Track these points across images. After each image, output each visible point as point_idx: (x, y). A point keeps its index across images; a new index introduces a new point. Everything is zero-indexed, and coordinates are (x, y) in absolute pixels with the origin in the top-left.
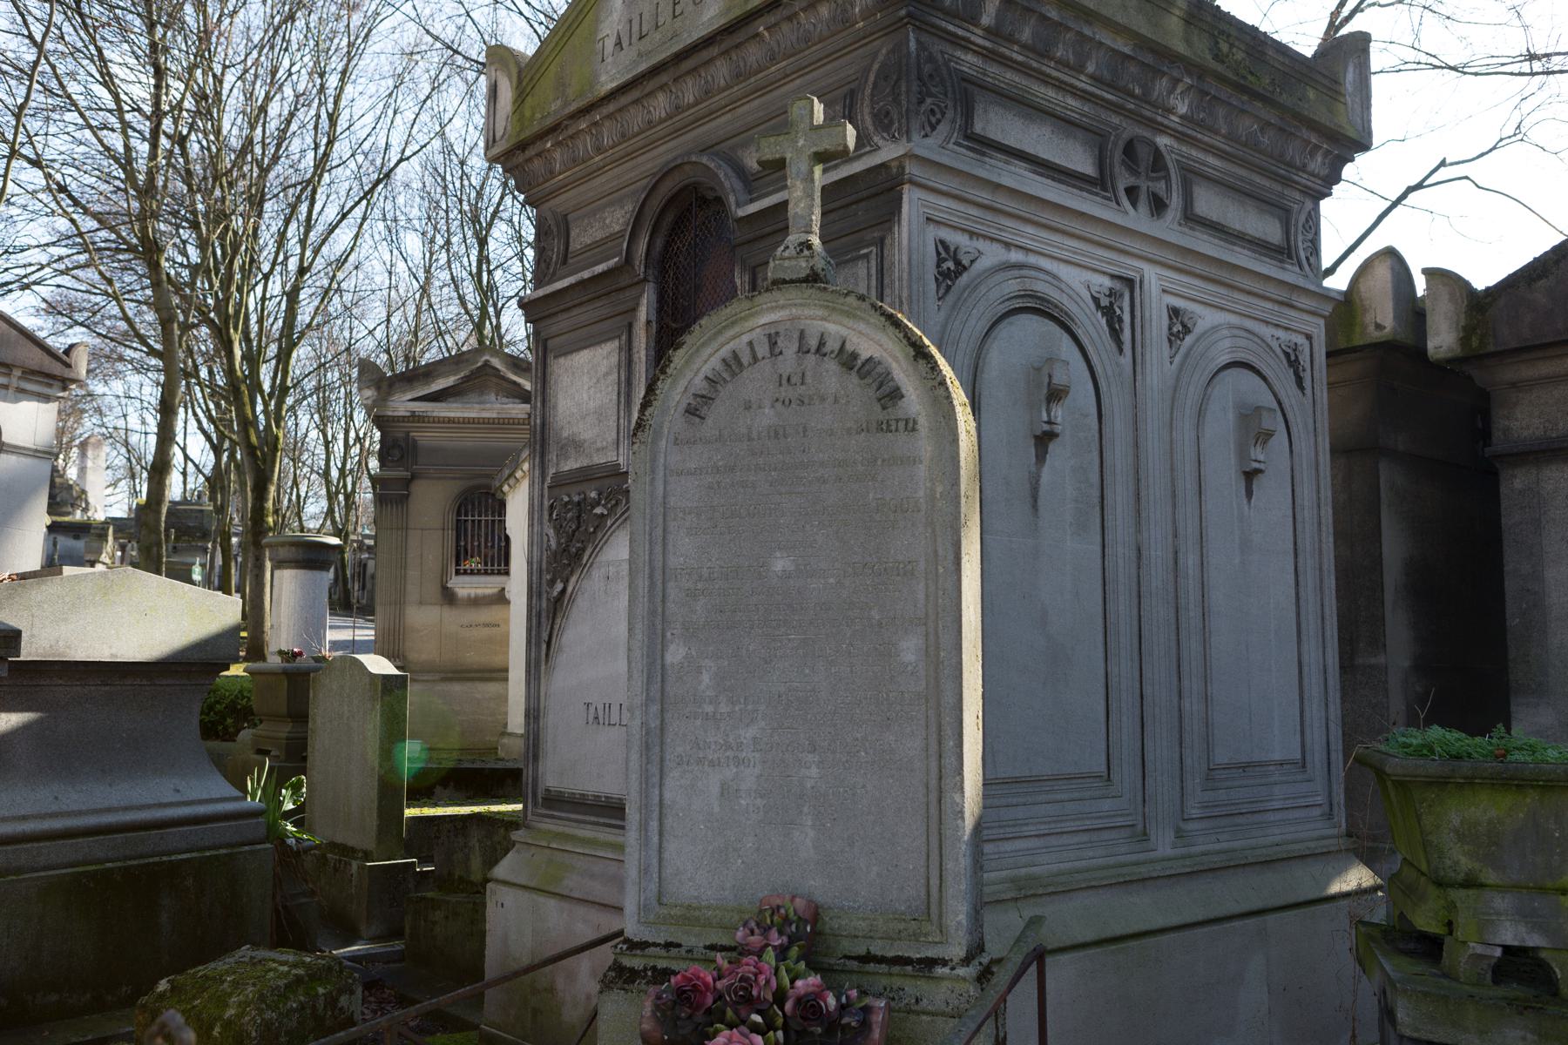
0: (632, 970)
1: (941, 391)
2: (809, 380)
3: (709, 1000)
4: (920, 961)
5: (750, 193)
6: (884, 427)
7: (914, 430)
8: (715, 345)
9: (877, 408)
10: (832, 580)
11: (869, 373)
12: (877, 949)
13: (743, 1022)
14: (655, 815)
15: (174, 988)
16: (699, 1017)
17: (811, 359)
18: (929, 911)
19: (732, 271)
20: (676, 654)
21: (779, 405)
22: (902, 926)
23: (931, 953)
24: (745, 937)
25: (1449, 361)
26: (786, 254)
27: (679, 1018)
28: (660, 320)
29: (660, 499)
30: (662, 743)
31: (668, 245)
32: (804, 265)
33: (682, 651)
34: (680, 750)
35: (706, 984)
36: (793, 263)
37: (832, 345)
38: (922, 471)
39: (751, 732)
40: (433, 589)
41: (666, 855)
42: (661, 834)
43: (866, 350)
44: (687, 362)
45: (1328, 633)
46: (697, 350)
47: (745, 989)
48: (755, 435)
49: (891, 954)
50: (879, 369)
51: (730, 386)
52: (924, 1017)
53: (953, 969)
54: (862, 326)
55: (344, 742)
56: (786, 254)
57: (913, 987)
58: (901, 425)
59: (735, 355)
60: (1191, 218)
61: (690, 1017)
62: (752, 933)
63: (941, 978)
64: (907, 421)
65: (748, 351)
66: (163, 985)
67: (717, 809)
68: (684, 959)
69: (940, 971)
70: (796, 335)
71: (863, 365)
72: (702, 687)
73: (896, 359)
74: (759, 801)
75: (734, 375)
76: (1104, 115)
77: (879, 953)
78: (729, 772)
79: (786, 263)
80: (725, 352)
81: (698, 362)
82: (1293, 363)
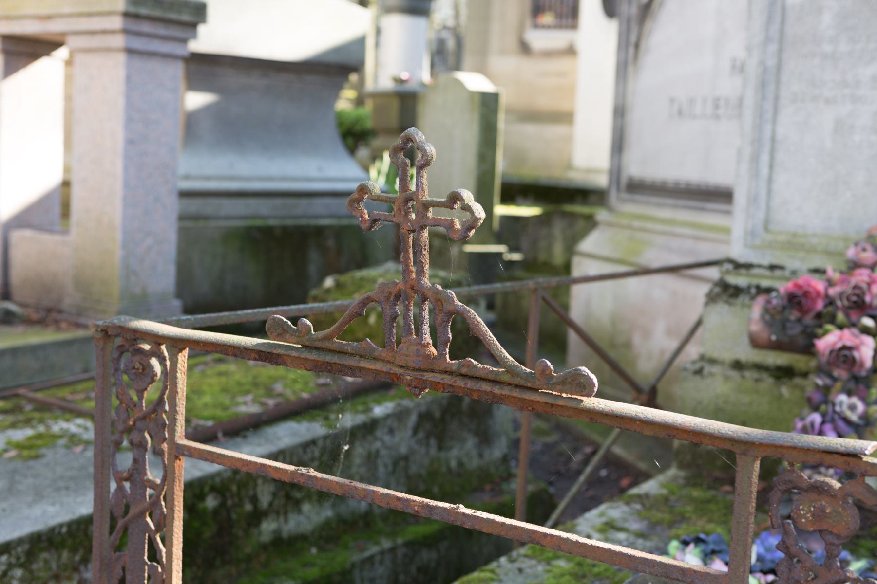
3: (820, 305)
13: (853, 325)
14: (767, 149)
15: (339, 286)
16: (809, 320)
24: (857, 254)
27: (788, 320)
40: (512, 41)
42: (771, 167)
47: (858, 296)
61: (799, 320)
62: (864, 250)
66: (329, 282)
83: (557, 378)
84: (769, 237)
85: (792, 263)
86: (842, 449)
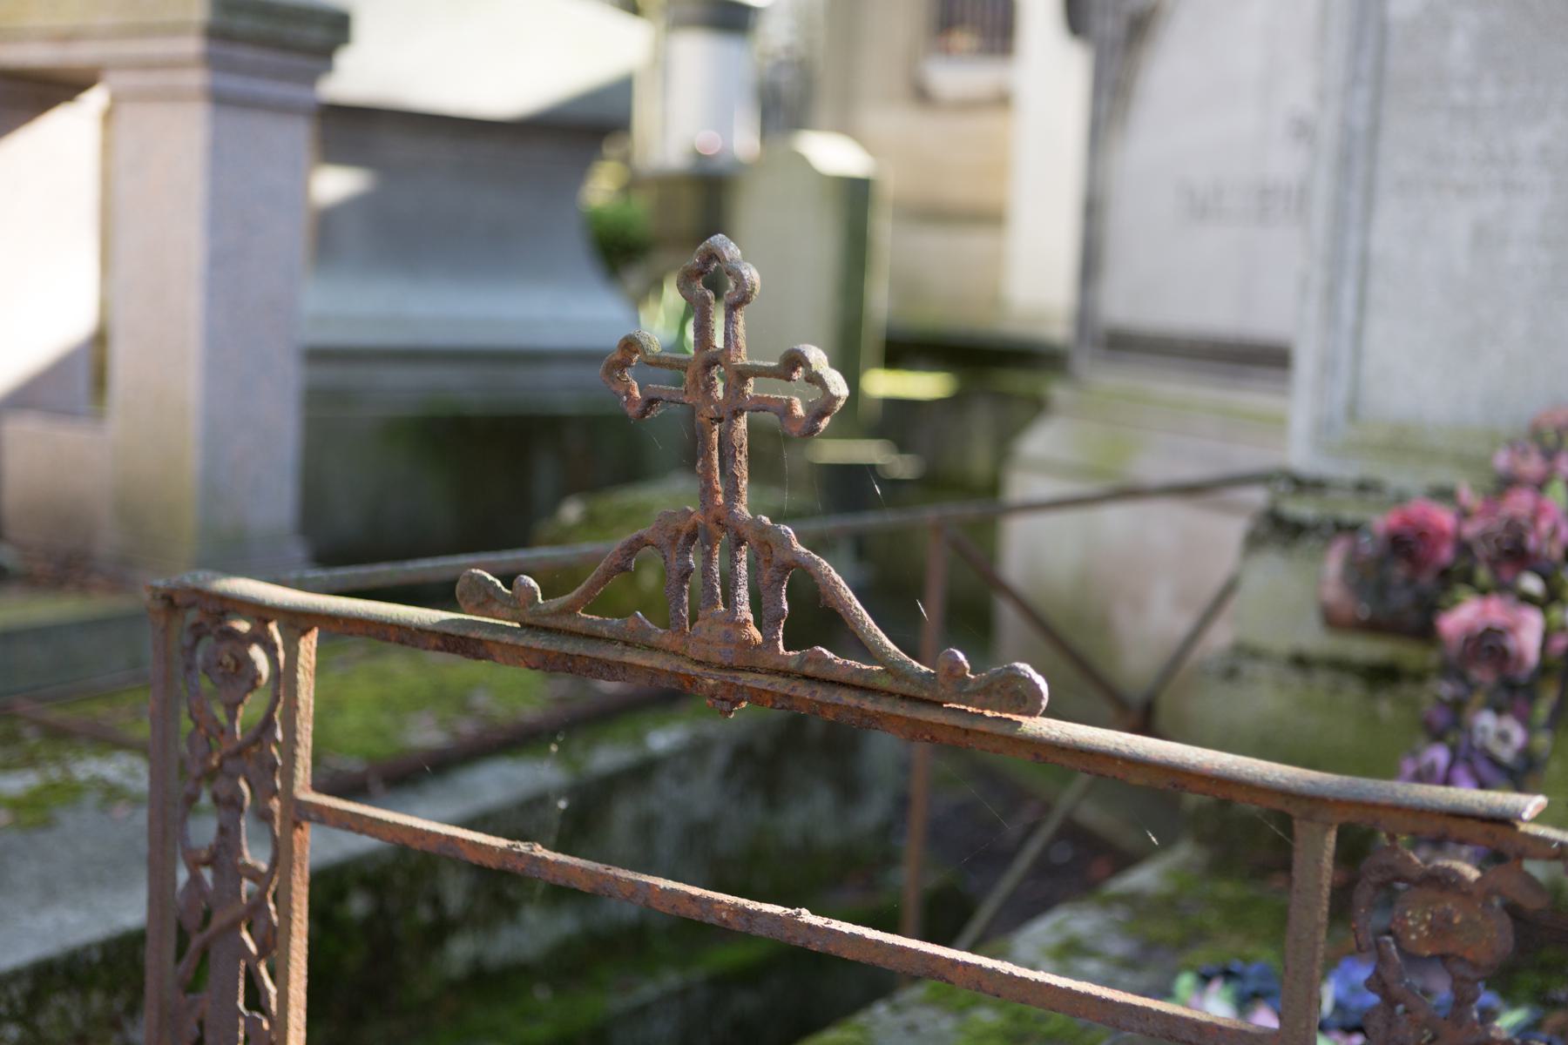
16: (1427, 580)
55: (779, 265)
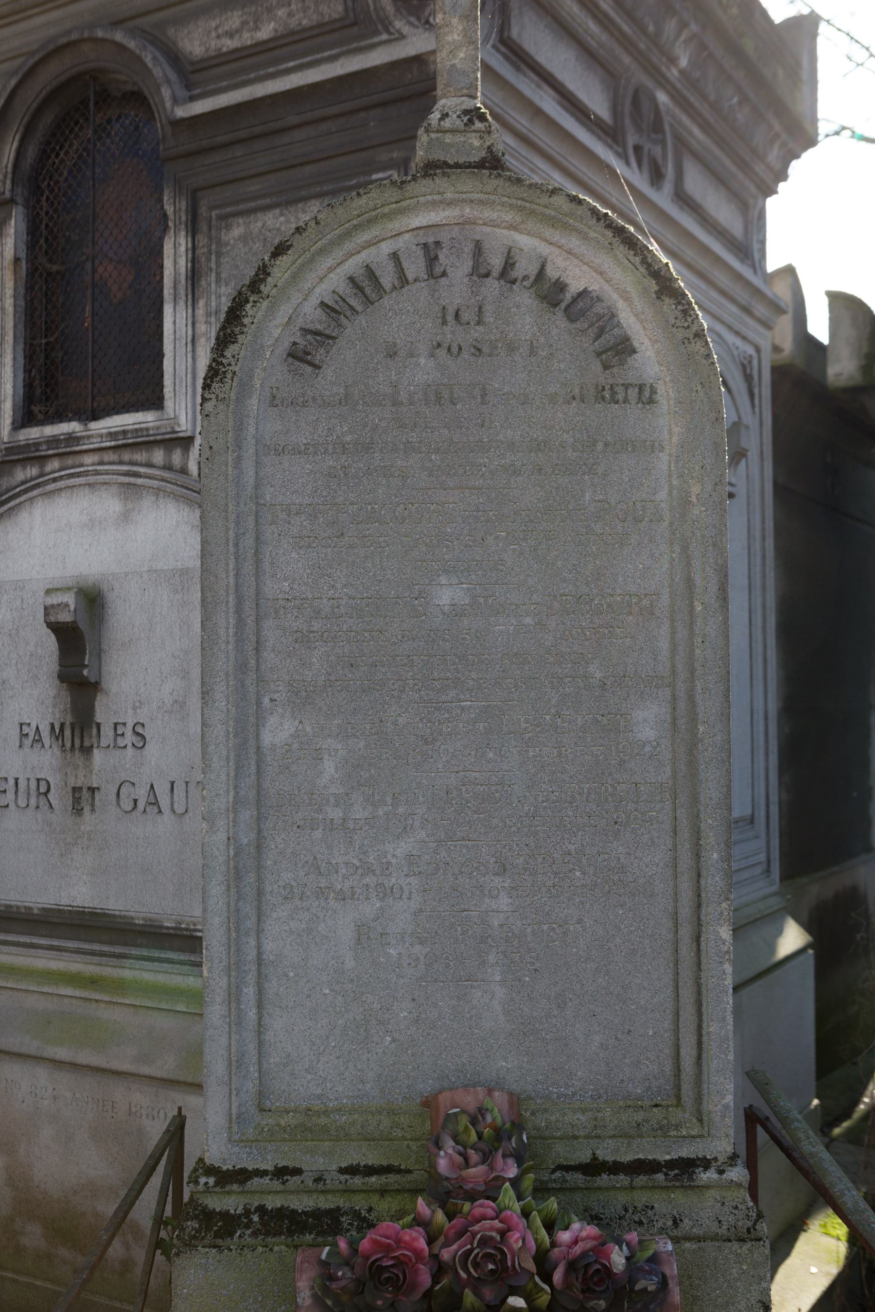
0: (225, 1215)
1: (698, 346)
2: (489, 318)
4: (671, 1164)
5: (188, 87)
6: (606, 395)
7: (651, 401)
8: (338, 254)
9: (596, 366)
10: (528, 620)
11: (583, 313)
12: (607, 1152)
14: (251, 978)
17: (492, 287)
18: (682, 1090)
19: (160, 200)
20: (278, 730)
21: (442, 353)
22: (639, 1117)
23: (686, 1152)
25: (846, 390)
26: (447, 124)
28: (32, 258)
29: (250, 490)
30: (259, 867)
31: (44, 155)
32: (476, 143)
33: (290, 726)
34: (287, 876)
35: (418, 1253)
36: (460, 138)
37: (525, 268)
38: (663, 461)
39: (402, 848)
41: (269, 1037)
42: (260, 1006)
43: (577, 278)
44: (294, 277)
45: (769, 676)
46: (311, 260)
48: (403, 396)
49: (627, 1157)
50: (599, 309)
51: (361, 320)
52: (687, 1245)
53: (721, 1172)
54: (574, 242)
56: (447, 124)
57: (666, 1202)
58: (633, 393)
59: (370, 272)
60: (682, 198)
63: (707, 1187)
64: (641, 388)
65: (391, 267)
67: (350, 964)
68: (309, 1192)
69: (708, 1176)
70: (469, 248)
71: (575, 300)
72: (324, 780)
73: (627, 299)
74: (417, 949)
75: (368, 302)
76: (619, 51)
77: (610, 1158)
78: (370, 908)
79: (448, 138)
80: (353, 266)
81: (311, 278)
82: (748, 378)
83: (599, 1299)
84: (269, 1121)
85: (313, 1162)
86: (710, 233)
